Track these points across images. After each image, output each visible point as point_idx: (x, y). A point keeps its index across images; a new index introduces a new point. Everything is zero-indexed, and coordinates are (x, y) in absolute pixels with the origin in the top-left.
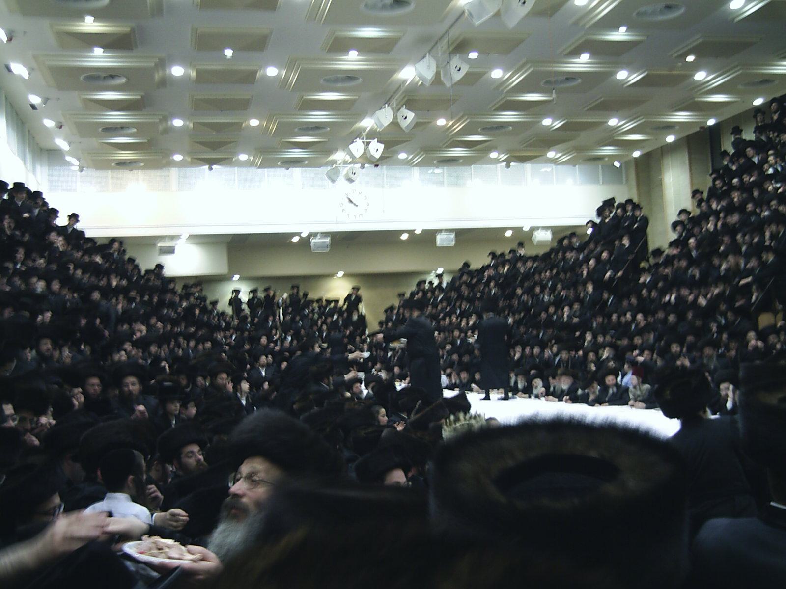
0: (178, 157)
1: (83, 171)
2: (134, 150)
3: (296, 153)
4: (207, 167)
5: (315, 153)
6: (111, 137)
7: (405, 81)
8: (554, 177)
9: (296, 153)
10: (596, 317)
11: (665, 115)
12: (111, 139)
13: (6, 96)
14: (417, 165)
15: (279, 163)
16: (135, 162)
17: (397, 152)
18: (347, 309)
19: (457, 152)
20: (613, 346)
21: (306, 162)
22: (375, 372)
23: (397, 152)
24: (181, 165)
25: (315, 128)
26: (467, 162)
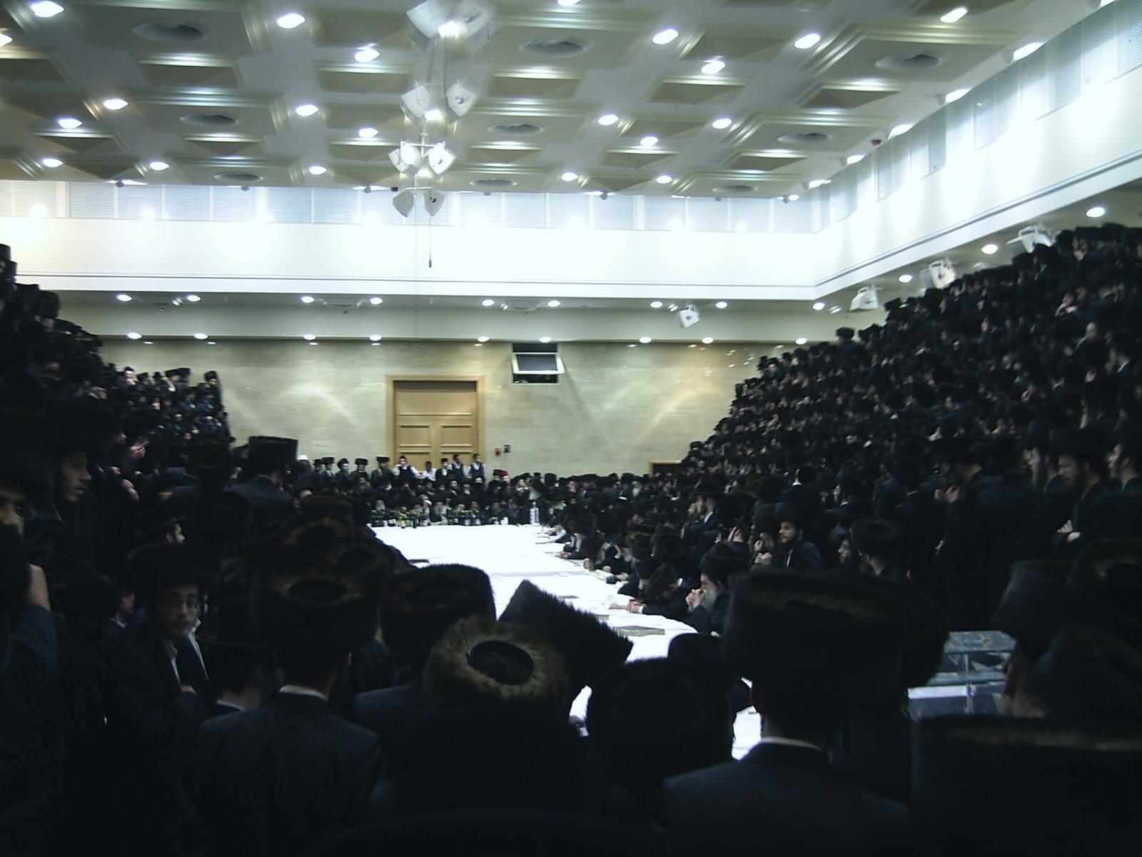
0: (317, 170)
1: (608, 199)
2: (766, 170)
3: (498, 169)
4: (363, 188)
5: (254, 163)
6: (758, 148)
7: (374, 48)
8: (313, 206)
9: (498, 169)
10: (749, 464)
11: (170, 95)
12: (757, 150)
13: (742, 86)
14: (686, 194)
15: (471, 183)
16: (732, 187)
17: (297, 159)
18: (867, 440)
19: (750, 175)
20: (575, 495)
21: (515, 184)
22: (444, 511)
23: (656, 174)
24: (318, 182)
25: (524, 127)
26: (766, 191)
